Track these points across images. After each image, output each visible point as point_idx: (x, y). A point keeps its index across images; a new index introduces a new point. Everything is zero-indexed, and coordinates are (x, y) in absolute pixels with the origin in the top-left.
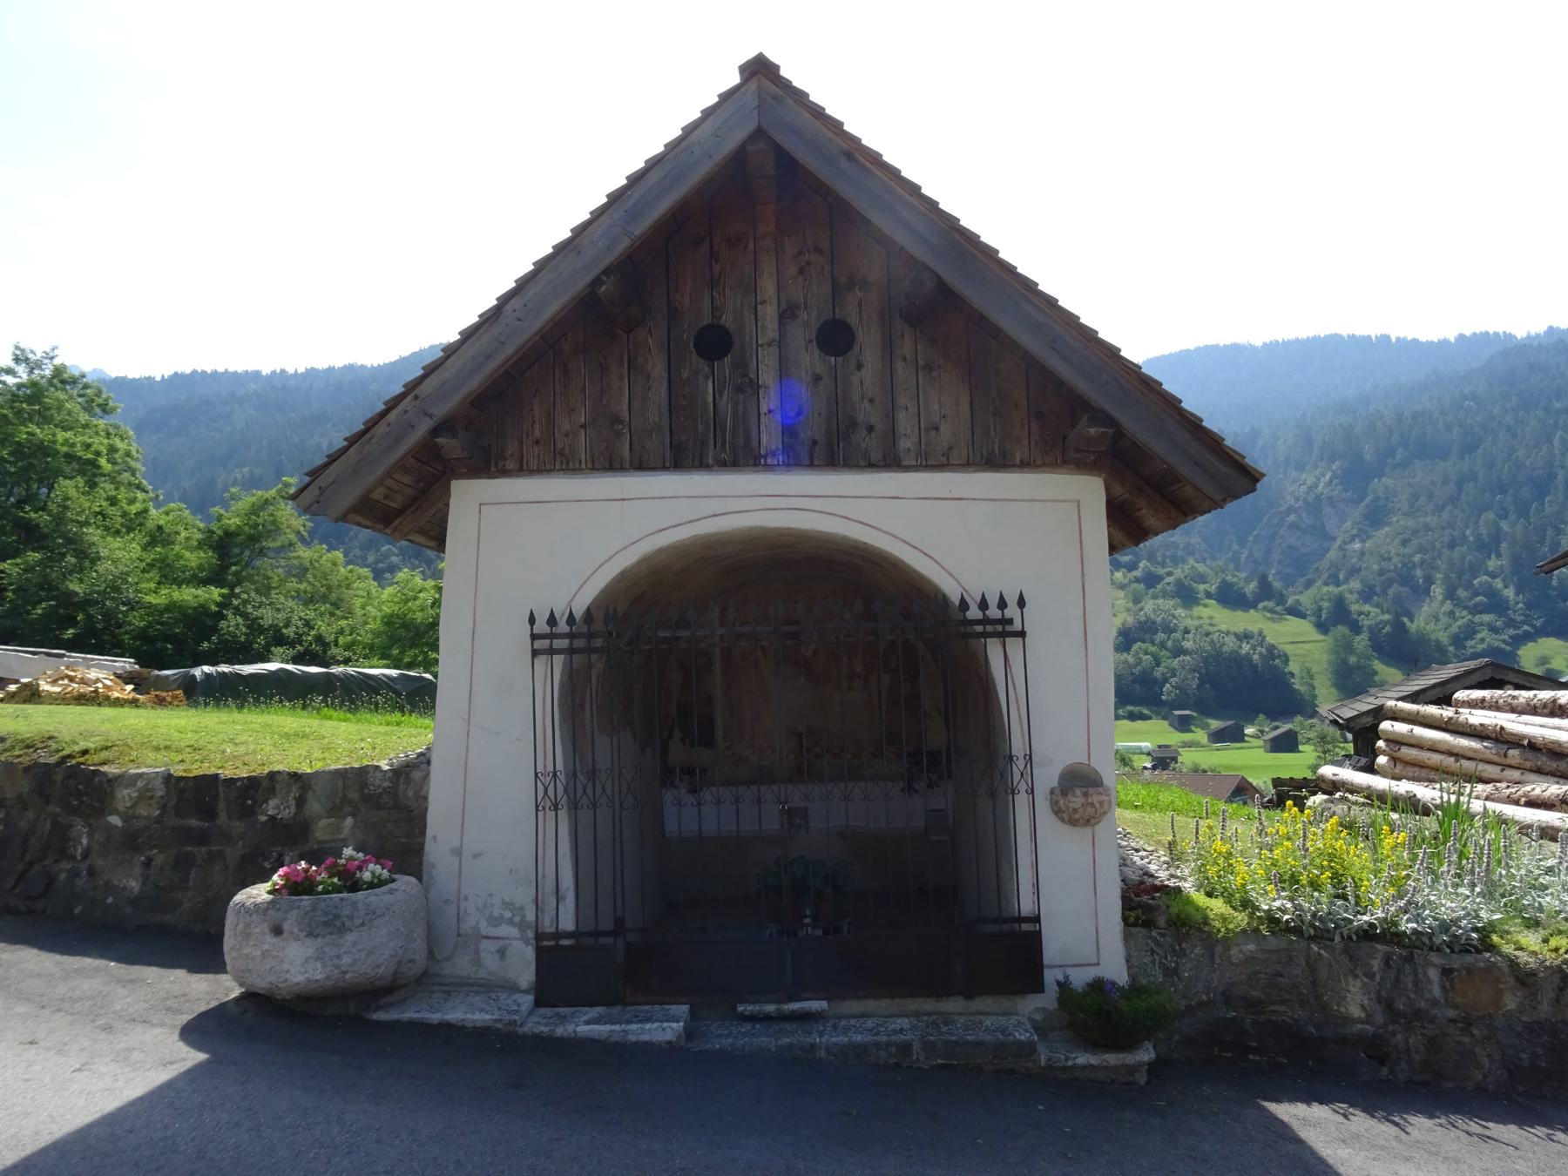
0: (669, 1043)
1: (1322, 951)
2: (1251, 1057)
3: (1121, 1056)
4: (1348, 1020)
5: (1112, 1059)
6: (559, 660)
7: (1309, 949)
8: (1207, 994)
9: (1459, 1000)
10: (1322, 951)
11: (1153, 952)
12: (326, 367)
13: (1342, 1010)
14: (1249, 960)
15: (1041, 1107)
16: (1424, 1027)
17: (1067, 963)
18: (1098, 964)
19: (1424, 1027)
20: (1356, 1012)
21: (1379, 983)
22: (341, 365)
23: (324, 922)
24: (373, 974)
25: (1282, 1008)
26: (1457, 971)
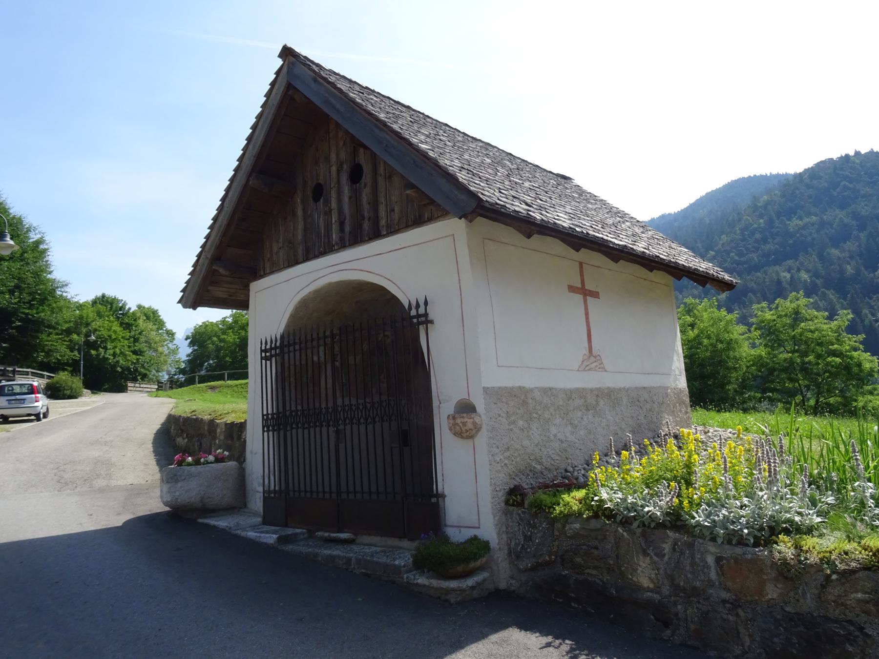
0: (272, 544)
1: (625, 534)
2: (573, 604)
3: (439, 582)
4: (639, 588)
5: (435, 583)
6: (274, 359)
7: (617, 531)
8: (550, 556)
9: (729, 584)
10: (625, 534)
11: (519, 524)
12: (650, 219)
13: (634, 579)
14: (576, 535)
15: (360, 599)
16: (699, 603)
17: (461, 525)
18: (479, 528)
19: (699, 603)
20: (645, 582)
21: (667, 563)
22: (658, 216)
23: (755, 536)
24: (189, 501)
25: (594, 572)
26: (726, 559)
